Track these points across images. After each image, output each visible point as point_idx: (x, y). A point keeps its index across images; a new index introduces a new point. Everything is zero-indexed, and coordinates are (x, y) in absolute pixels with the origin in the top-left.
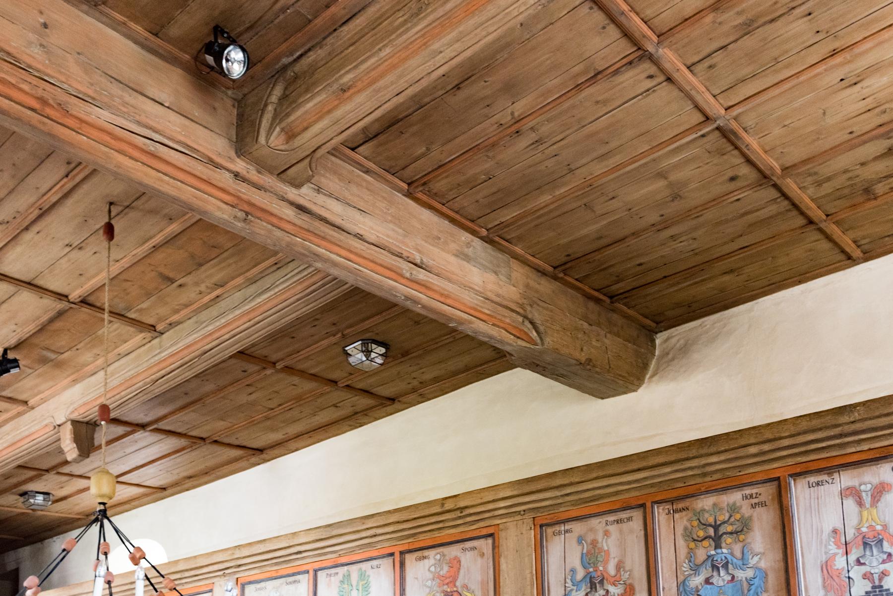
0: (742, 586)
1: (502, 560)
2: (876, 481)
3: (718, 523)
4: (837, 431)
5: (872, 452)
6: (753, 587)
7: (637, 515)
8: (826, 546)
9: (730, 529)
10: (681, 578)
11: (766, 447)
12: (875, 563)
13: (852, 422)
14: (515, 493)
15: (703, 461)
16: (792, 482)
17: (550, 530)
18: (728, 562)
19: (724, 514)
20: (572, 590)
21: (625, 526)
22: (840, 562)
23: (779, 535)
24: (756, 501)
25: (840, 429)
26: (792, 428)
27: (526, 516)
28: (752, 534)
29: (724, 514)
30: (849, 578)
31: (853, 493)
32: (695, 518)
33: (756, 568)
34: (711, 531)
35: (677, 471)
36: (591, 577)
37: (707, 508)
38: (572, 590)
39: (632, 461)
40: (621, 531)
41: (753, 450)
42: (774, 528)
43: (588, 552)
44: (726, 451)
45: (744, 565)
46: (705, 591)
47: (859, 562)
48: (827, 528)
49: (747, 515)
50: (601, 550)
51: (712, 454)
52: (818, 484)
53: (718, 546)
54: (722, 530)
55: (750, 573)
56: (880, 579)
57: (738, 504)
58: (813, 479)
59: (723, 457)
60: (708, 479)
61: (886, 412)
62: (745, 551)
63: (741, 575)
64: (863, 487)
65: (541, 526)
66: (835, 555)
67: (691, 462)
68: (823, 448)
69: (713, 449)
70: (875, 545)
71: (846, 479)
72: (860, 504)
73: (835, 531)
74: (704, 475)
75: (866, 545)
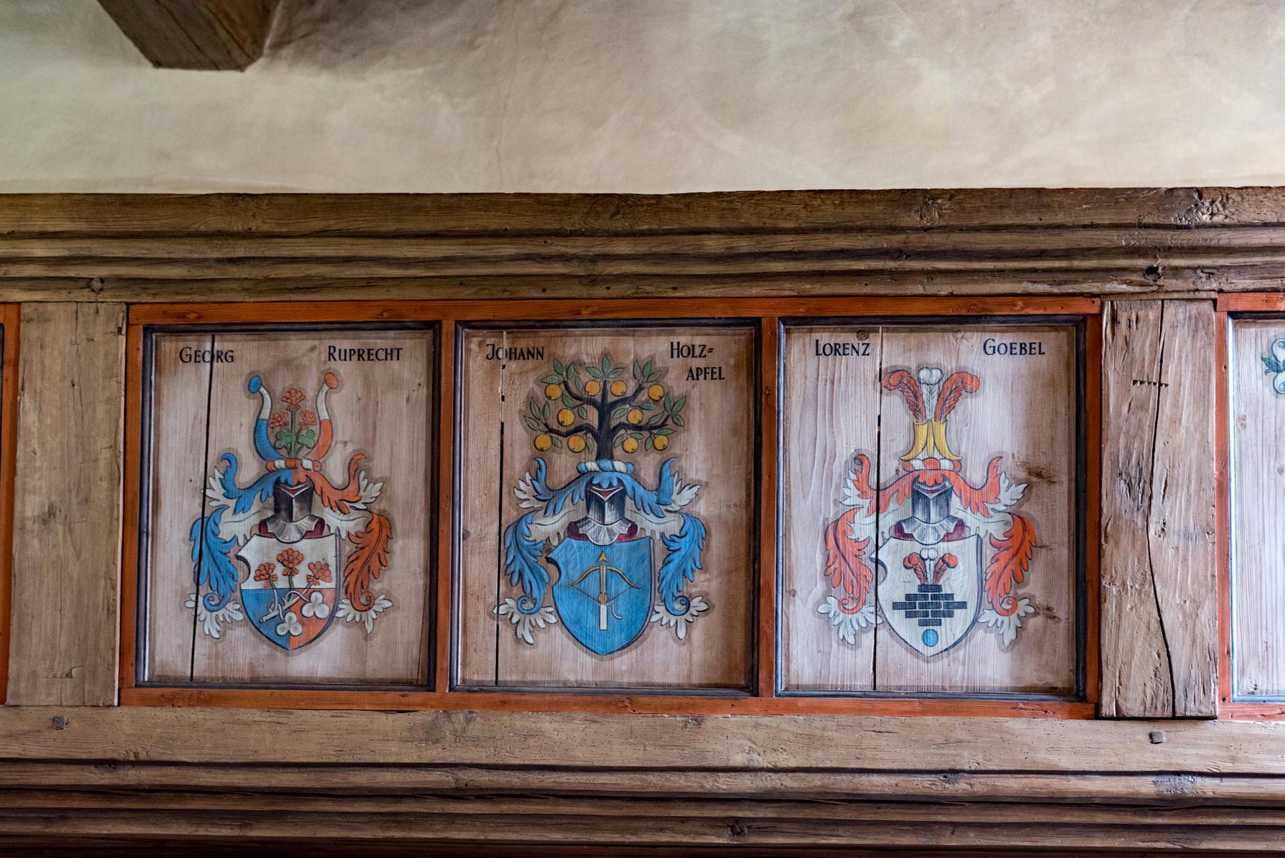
0: (651, 550)
1: (27, 402)
2: (950, 366)
3: (611, 399)
4: (895, 240)
5: (953, 302)
6: (676, 558)
7: (414, 350)
8: (838, 488)
9: (635, 417)
10: (510, 515)
11: (744, 244)
12: (931, 539)
13: (926, 229)
14: (82, 226)
15: (598, 246)
16: (783, 336)
17: (169, 346)
18: (623, 493)
19: (625, 382)
20: (224, 507)
21: (378, 369)
22: (863, 527)
23: (741, 449)
24: (700, 363)
25: (901, 237)
26: (803, 214)
27: (106, 296)
28: (683, 436)
29: (625, 382)
30: (877, 561)
31: (900, 382)
32: (556, 379)
33: (685, 514)
34: (593, 416)
35: (530, 257)
36: (278, 482)
37: (585, 359)
38: (224, 507)
39: (418, 210)
40: (367, 381)
41: (713, 244)
42: (735, 431)
43: (274, 419)
44: (651, 233)
45: (660, 505)
46: (568, 552)
47: (899, 532)
48: (845, 451)
49: (676, 393)
50: (311, 418)
51: (617, 235)
52: (836, 350)
53: (604, 453)
54: (617, 417)
55: (672, 525)
56: (938, 574)
57: (659, 364)
58: (826, 338)
59: (643, 247)
60: (600, 291)
61: (992, 222)
62: (666, 474)
63: (651, 525)
64: (924, 374)
65: (148, 330)
66: (855, 509)
67: (570, 242)
68: (859, 273)
69: (621, 224)
70: (936, 500)
71: (890, 350)
72: (915, 408)
73: (859, 458)
74: (593, 280)
75: (917, 496)
